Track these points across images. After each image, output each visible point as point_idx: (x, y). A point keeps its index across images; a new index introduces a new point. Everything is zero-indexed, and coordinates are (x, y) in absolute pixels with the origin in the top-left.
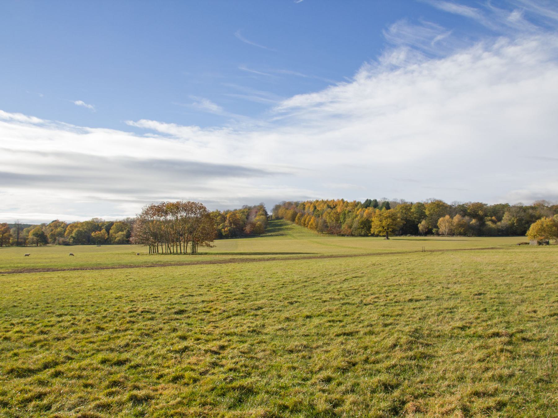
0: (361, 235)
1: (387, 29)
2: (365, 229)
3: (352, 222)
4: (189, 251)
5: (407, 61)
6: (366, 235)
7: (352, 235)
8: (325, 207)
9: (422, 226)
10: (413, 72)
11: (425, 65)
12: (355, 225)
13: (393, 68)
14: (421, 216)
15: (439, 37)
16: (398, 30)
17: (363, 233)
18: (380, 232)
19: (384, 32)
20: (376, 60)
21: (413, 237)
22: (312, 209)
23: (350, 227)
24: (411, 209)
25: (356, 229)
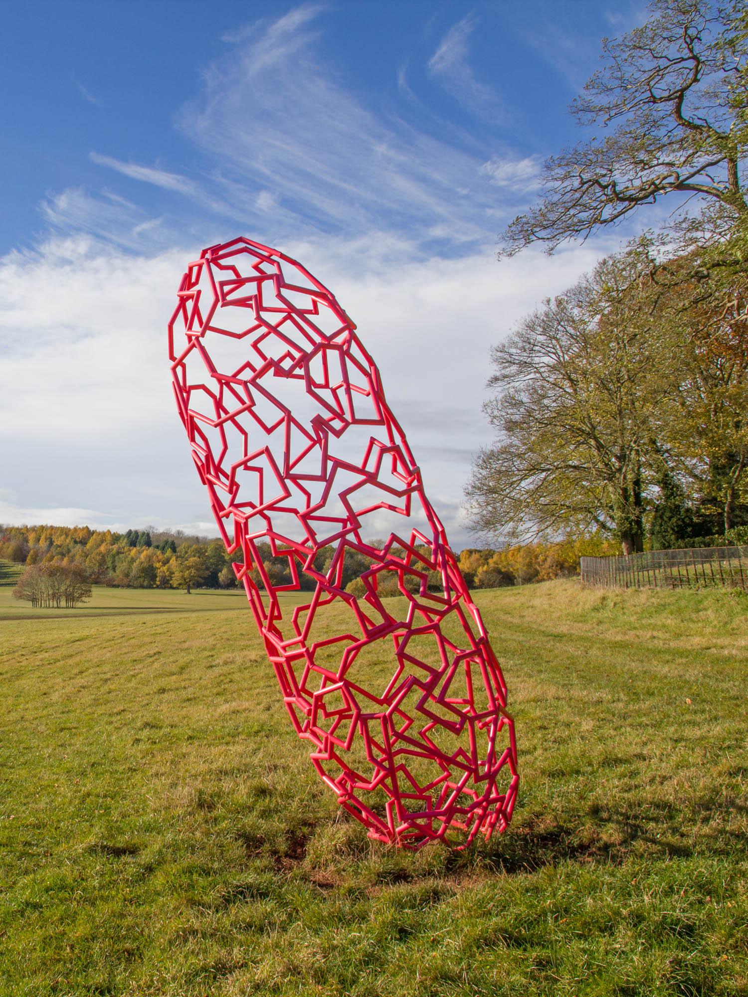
0: (142, 587)
1: (51, 203)
2: (149, 578)
3: (130, 568)
4: (55, 605)
5: (91, 255)
6: (150, 587)
7: (129, 586)
8: (68, 541)
9: (223, 576)
10: (97, 271)
11: (117, 262)
12: (134, 573)
13: (64, 262)
14: (218, 561)
15: (146, 226)
16: (67, 203)
17: (145, 584)
18: (180, 584)
19: (44, 204)
20: (31, 249)
21: (212, 591)
22: (43, 544)
23: (127, 575)
24: (206, 551)
25: (137, 578)
